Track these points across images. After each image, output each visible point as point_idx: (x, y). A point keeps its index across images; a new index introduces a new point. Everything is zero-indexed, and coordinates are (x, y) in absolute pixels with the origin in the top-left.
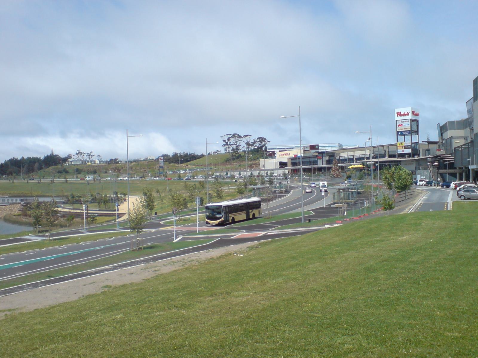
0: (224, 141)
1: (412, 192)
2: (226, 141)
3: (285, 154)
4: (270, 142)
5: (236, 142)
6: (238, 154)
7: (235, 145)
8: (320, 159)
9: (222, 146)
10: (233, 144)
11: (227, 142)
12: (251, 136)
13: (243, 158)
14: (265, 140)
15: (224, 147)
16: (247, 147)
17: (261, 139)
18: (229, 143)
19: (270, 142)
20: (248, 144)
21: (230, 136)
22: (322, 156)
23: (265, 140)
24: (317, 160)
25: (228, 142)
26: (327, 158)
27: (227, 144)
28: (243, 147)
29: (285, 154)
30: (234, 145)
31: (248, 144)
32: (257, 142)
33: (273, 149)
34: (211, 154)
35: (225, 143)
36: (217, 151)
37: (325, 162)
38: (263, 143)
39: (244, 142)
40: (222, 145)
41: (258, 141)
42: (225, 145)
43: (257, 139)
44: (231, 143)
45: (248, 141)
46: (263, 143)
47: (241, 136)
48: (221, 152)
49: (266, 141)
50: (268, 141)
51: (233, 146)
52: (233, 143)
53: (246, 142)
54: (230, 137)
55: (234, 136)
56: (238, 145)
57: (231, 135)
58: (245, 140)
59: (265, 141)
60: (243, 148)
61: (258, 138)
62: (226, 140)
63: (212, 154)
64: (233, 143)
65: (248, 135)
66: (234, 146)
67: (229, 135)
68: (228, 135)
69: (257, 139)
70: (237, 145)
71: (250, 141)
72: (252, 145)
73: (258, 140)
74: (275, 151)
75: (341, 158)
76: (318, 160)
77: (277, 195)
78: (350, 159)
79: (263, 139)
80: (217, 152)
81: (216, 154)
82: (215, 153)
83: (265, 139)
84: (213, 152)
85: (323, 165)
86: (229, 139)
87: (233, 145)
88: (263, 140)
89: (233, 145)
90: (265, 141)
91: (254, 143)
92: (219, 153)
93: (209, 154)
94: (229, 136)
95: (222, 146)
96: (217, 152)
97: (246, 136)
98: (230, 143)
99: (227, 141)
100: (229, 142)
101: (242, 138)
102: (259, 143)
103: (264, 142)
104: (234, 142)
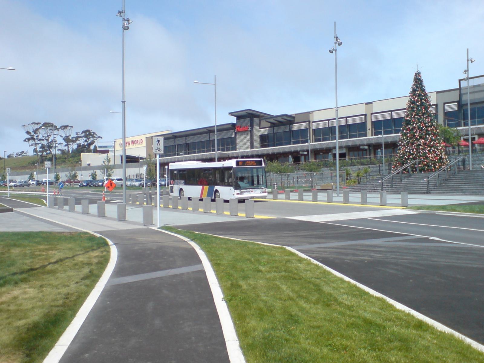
0: (28, 133)
1: (423, 254)
2: (31, 133)
3: (133, 143)
4: (102, 138)
5: (48, 136)
6: (51, 154)
7: (46, 140)
8: (244, 132)
9: (25, 141)
10: (43, 138)
11: (32, 136)
12: (73, 127)
13: (59, 160)
14: (95, 135)
15: (27, 143)
16: (66, 144)
17: (87, 133)
18: (36, 137)
19: (102, 138)
20: (67, 140)
21: (39, 126)
22: (252, 126)
23: (93, 134)
24: (233, 136)
25: (34, 136)
26: (265, 131)
27: (33, 139)
28: (59, 144)
29: (133, 143)
30: (45, 140)
31: (67, 140)
32: (80, 137)
33: (106, 147)
34: (13, 157)
35: (29, 136)
36: (21, 152)
37: (257, 142)
38: (91, 139)
39: (61, 136)
40: (24, 139)
41: (83, 136)
42: (29, 139)
43: (82, 134)
44: (40, 137)
45: (68, 135)
46: (91, 139)
47: (56, 127)
48: (28, 154)
49: (96, 137)
50: (100, 137)
51: (42, 142)
52: (43, 137)
53: (64, 136)
54: (39, 127)
55: (47, 125)
56: (52, 141)
57: (41, 125)
58: (63, 133)
59: (93, 137)
60: (60, 145)
61: (83, 132)
62: (31, 131)
63: (14, 157)
64: (43, 137)
65: (67, 126)
66: (45, 143)
67: (36, 125)
68: (35, 123)
69: (82, 134)
70: (50, 140)
71: (70, 135)
72: (74, 141)
73: (83, 134)
74: (110, 149)
75: (315, 126)
76: (239, 138)
77: (322, 137)
78: (349, 125)
79: (90, 133)
80: (21, 154)
81: (21, 156)
82: (20, 155)
83: (94, 133)
84: (16, 154)
85: (252, 147)
86: (35, 131)
87: (43, 140)
88: (90, 134)
89: (43, 140)
90: (93, 137)
91: (77, 138)
92: (25, 154)
93: (9, 156)
94: (36, 126)
95: (25, 141)
96: (21, 154)
97: (65, 127)
98: (38, 136)
99: (32, 134)
100: (37, 135)
101: (58, 129)
102: (85, 139)
103: (92, 137)
104: (46, 135)
